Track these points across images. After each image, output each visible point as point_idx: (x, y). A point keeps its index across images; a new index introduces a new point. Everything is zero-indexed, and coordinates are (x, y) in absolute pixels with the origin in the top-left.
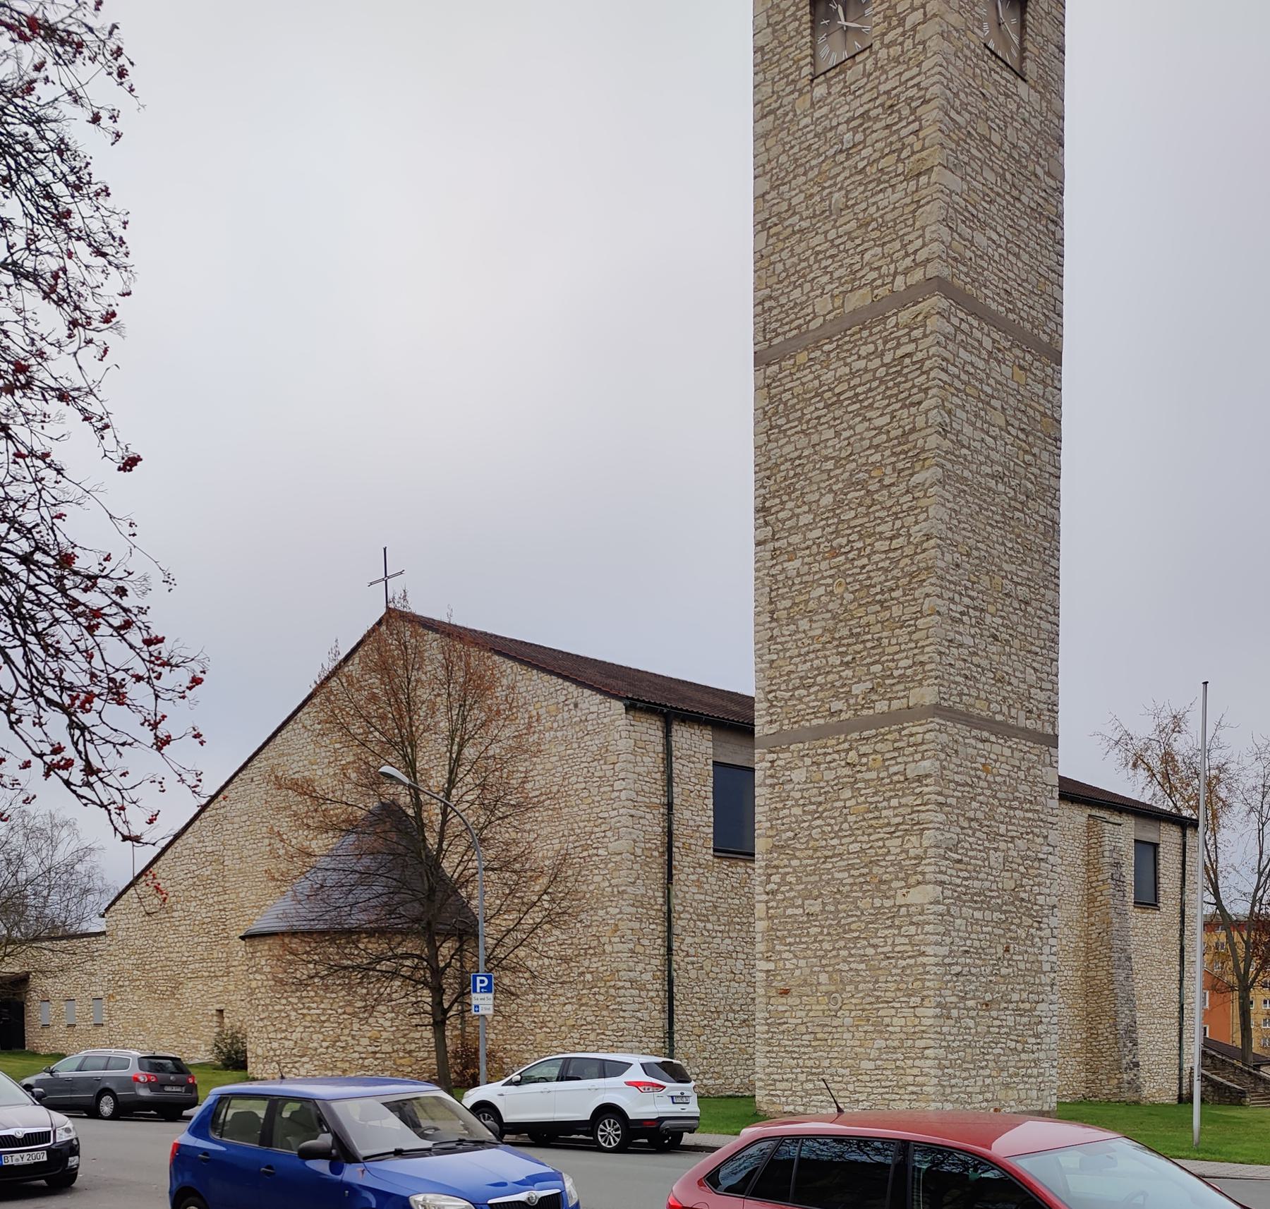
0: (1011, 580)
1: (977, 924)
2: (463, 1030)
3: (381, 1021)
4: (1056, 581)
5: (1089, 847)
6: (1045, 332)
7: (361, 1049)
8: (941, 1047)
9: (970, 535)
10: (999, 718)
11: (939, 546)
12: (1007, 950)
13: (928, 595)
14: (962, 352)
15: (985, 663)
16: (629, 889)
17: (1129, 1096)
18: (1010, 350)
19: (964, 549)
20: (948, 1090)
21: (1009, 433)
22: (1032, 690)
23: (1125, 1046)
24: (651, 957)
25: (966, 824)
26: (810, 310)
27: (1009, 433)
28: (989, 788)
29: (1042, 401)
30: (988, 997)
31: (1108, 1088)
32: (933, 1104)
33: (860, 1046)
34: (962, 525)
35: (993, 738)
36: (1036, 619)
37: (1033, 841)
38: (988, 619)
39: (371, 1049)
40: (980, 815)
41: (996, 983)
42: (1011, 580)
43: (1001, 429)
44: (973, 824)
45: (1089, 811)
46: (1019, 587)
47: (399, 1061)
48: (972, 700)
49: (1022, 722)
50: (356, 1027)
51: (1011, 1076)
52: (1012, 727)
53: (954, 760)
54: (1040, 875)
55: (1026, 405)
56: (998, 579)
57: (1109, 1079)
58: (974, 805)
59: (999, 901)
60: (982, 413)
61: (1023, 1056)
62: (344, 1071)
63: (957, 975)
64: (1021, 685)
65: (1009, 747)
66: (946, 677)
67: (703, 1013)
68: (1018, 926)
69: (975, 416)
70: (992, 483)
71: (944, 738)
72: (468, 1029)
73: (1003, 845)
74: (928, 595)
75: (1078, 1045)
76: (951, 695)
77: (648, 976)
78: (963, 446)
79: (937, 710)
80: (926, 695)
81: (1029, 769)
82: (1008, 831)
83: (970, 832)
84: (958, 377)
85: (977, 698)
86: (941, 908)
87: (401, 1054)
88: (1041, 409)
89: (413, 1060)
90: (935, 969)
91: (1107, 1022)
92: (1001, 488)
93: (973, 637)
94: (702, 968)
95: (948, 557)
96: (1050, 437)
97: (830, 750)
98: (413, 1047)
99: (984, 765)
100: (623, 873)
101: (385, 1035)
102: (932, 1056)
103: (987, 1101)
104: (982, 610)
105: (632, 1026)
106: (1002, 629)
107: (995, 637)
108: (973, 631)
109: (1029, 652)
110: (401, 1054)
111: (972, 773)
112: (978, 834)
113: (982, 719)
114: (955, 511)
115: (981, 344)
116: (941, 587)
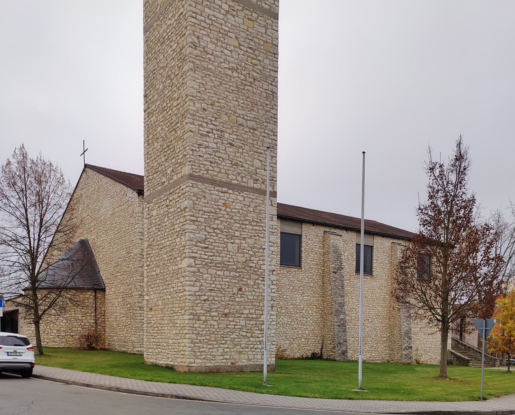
1: (219, 277)
2: (96, 327)
3: (61, 323)
4: (275, 120)
5: (392, 256)
6: (266, 4)
7: (53, 334)
8: (193, 334)
9: (214, 95)
10: (234, 182)
11: (191, 100)
12: (240, 290)
13: (187, 123)
14: (207, 10)
15: (224, 156)
16: (139, 269)
17: (405, 360)
18: (242, 11)
19: (210, 102)
21: (241, 50)
22: (258, 170)
23: (404, 339)
25: (211, 231)
26: (156, 4)
27: (241, 50)
28: (228, 214)
29: (264, 36)
30: (227, 311)
31: (397, 357)
32: (188, 360)
33: (169, 333)
34: (208, 91)
35: (231, 191)
36: (261, 137)
37: (259, 240)
38: (227, 136)
39: (57, 334)
40: (220, 227)
41: (232, 305)
42: (243, 118)
43: (235, 47)
44: (216, 231)
45: (392, 240)
46: (248, 122)
47: (68, 339)
48: (215, 173)
49: (251, 184)
50: (52, 325)
51: (243, 348)
52: (244, 187)
53: (203, 200)
55: (253, 37)
56: (233, 117)
57: (397, 353)
58: (217, 222)
59: (235, 267)
60: (222, 39)
61: (251, 339)
62: (47, 343)
63: (205, 300)
64: (251, 168)
65: (242, 196)
66: (197, 161)
68: (248, 279)
69: (217, 40)
70: (230, 72)
71: (196, 190)
72: (98, 327)
73: (237, 241)
74: (187, 123)
75: (385, 339)
76: (200, 170)
78: (209, 54)
79: (191, 177)
80: (186, 170)
81: (256, 207)
82: (241, 235)
83: (214, 234)
84: (205, 21)
85: (220, 172)
86: (193, 269)
87: (69, 337)
88: (265, 39)
89: (74, 339)
90: (190, 297)
91: (397, 329)
92: (235, 74)
93: (216, 143)
95: (198, 105)
96: (270, 52)
97: (162, 200)
98: (74, 334)
99: (224, 204)
100: (137, 263)
101: (62, 329)
102: (187, 337)
103: (225, 359)
104: (222, 131)
105: (140, 326)
106: (237, 141)
107: (231, 144)
108: (216, 141)
109: (256, 152)
110: (69, 337)
111: (216, 207)
112: (219, 235)
113: (223, 182)
114: (203, 84)
115: (221, 7)
116: (194, 119)
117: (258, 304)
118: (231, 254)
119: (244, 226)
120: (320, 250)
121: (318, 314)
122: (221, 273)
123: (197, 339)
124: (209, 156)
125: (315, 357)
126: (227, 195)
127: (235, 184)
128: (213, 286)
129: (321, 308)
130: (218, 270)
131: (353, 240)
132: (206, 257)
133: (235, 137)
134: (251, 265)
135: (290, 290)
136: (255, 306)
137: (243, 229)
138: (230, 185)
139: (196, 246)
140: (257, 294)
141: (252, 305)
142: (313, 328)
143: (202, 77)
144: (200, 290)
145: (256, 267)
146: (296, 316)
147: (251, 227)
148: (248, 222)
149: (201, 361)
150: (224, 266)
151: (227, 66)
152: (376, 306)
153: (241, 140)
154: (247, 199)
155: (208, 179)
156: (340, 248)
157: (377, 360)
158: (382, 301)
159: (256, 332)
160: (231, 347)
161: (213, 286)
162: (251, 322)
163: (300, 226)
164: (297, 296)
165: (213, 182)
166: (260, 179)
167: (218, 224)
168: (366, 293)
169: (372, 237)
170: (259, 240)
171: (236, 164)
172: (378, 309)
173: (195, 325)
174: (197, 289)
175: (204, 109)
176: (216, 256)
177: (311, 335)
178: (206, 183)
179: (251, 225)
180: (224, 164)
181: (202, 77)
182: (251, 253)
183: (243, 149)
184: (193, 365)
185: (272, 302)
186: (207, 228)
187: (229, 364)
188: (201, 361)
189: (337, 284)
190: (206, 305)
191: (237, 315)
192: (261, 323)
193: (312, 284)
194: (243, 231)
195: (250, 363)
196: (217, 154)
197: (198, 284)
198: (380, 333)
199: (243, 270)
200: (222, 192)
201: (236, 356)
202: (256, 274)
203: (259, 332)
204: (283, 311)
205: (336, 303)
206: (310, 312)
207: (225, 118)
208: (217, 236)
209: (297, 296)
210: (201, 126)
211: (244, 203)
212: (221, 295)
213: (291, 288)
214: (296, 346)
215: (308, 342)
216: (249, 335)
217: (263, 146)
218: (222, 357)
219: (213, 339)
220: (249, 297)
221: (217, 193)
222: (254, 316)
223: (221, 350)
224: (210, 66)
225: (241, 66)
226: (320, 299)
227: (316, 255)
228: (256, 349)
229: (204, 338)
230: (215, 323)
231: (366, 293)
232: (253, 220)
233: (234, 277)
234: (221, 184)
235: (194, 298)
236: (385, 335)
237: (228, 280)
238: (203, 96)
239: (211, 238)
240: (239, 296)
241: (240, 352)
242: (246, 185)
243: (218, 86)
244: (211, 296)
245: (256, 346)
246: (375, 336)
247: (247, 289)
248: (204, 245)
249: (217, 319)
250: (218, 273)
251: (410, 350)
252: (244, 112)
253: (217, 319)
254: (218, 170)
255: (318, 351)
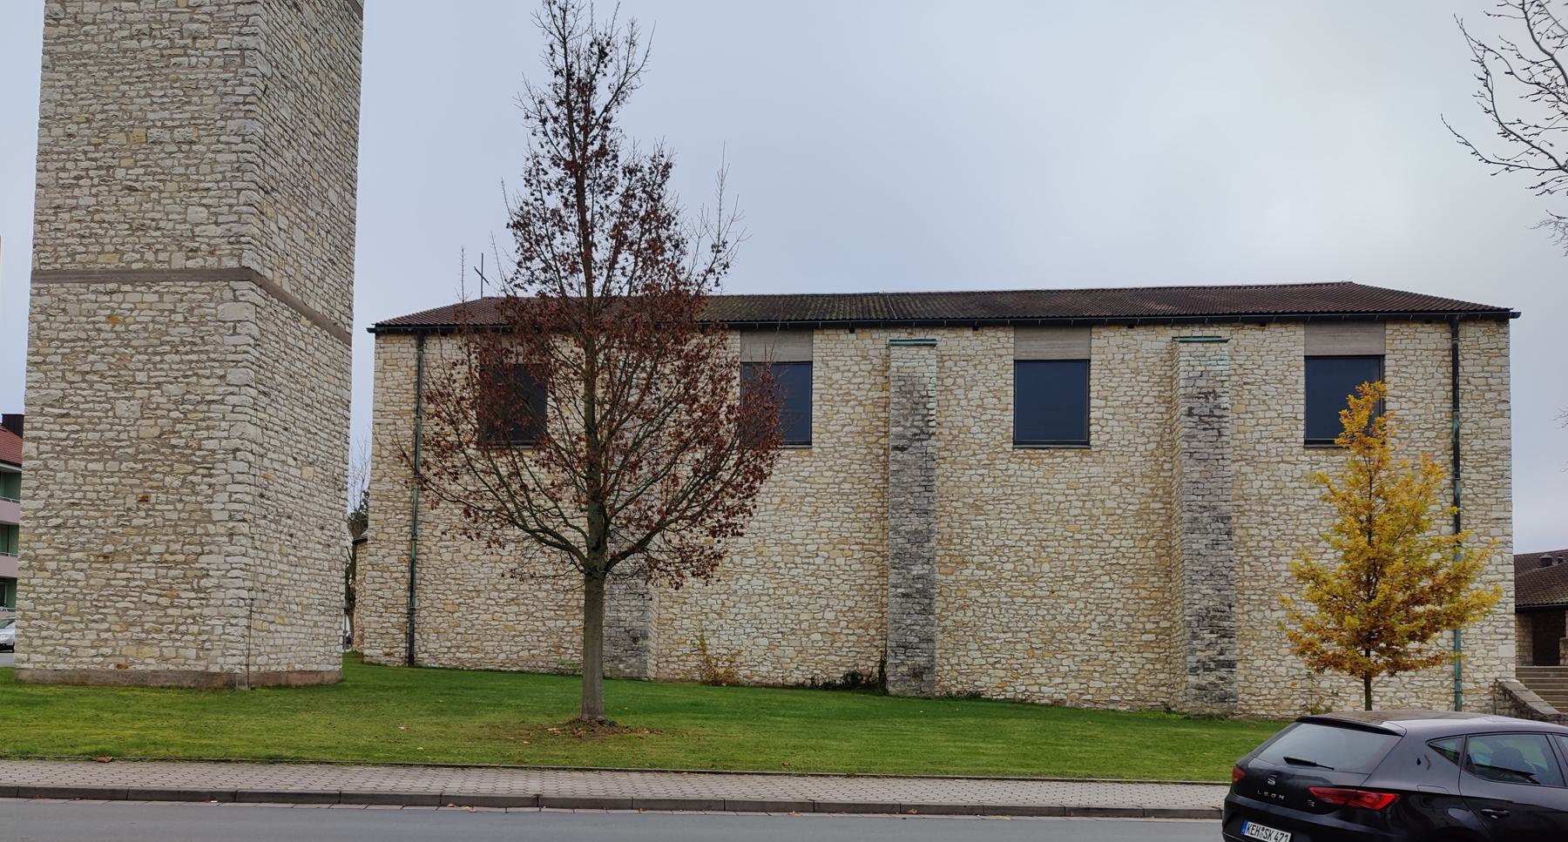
0: (163, 126)
10: (135, 266)
12: (145, 499)
20: (37, 642)
22: (197, 230)
24: (395, 542)
30: (109, 548)
35: (128, 288)
42: (163, 126)
45: (1173, 332)
49: (179, 261)
52: (162, 271)
54: (210, 418)
58: (91, 357)
61: (170, 611)
63: (57, 527)
64: (182, 227)
67: (458, 592)
70: (133, 44)
75: (1152, 637)
77: (393, 559)
83: (84, 385)
92: (146, 43)
93: (96, 196)
94: (459, 551)
99: (109, 317)
108: (94, 191)
109: (195, 190)
112: (96, 386)
113: (108, 272)
114: (69, 87)
117: (191, 531)
118: (124, 422)
119: (158, 358)
120: (876, 394)
121: (868, 567)
122: (98, 466)
123: (34, 610)
124: (77, 225)
125: (853, 683)
126: (117, 297)
127: (139, 271)
128: (78, 495)
129: (879, 549)
130: (92, 461)
131: (1003, 352)
132: (64, 435)
133: (142, 171)
134: (173, 442)
135: (770, 507)
136: (182, 534)
137: (154, 364)
138: (126, 276)
139: (41, 414)
140: (189, 508)
141: (175, 533)
142: (850, 603)
143: (69, 74)
144: (47, 505)
145: (187, 446)
146: (794, 572)
147: (177, 358)
148: (168, 348)
149: (43, 658)
150: (105, 451)
151: (126, 33)
152: (1106, 537)
153: (155, 174)
154: (167, 298)
155: (75, 272)
156: (926, 380)
157: (1113, 702)
158: (1131, 520)
159: (183, 594)
160: (118, 628)
161: (78, 495)
162: (172, 573)
163: (806, 338)
164: (796, 520)
165: (86, 276)
166: (204, 247)
167: (93, 363)
168: (1063, 499)
169: (1378, 329)
170: (197, 384)
171: (142, 227)
172: (1115, 543)
173: (33, 581)
174: (40, 504)
175: (70, 135)
176: (88, 431)
177: (843, 624)
178: (71, 280)
179: (177, 352)
180: (112, 233)
181: (69, 74)
182: (175, 414)
183: (161, 192)
184: (25, 665)
185: (231, 524)
186: (68, 374)
187: (112, 667)
188: (43, 658)
189: (905, 479)
190: (61, 538)
191: (135, 557)
192: (199, 573)
193: (846, 486)
194: (157, 370)
195: (164, 666)
196: (97, 217)
197: (43, 494)
198: (1129, 619)
199: (152, 456)
200: (107, 293)
201: (131, 651)
202: (187, 463)
203: (193, 595)
204: (748, 562)
205: (898, 533)
206: (841, 561)
207: (118, 138)
208: (91, 387)
209: (796, 520)
210: (64, 169)
211: (160, 306)
212: (98, 514)
213: (776, 500)
214: (790, 652)
215: (833, 642)
216: (164, 601)
217: (213, 172)
218: (94, 652)
219: (74, 611)
220: (168, 515)
221: (93, 297)
222: (181, 558)
223: (92, 636)
224: (86, 48)
225: (156, 21)
226: (877, 525)
227: (859, 409)
228: (183, 634)
229: (51, 608)
230: (81, 576)
231: (1063, 499)
232: (183, 342)
233: (131, 473)
234: (105, 276)
235: (33, 523)
236: (1149, 626)
237: (116, 480)
238: (70, 109)
239: (76, 395)
240: (142, 514)
241: (140, 642)
242: (166, 266)
243: (105, 79)
244: (73, 517)
245: (183, 628)
246: (1103, 627)
247: (163, 497)
248: (57, 411)
249: (85, 566)
250: (91, 466)
251: (1223, 672)
252: (166, 114)
253: (85, 566)
254: (97, 248)
255: (869, 666)
